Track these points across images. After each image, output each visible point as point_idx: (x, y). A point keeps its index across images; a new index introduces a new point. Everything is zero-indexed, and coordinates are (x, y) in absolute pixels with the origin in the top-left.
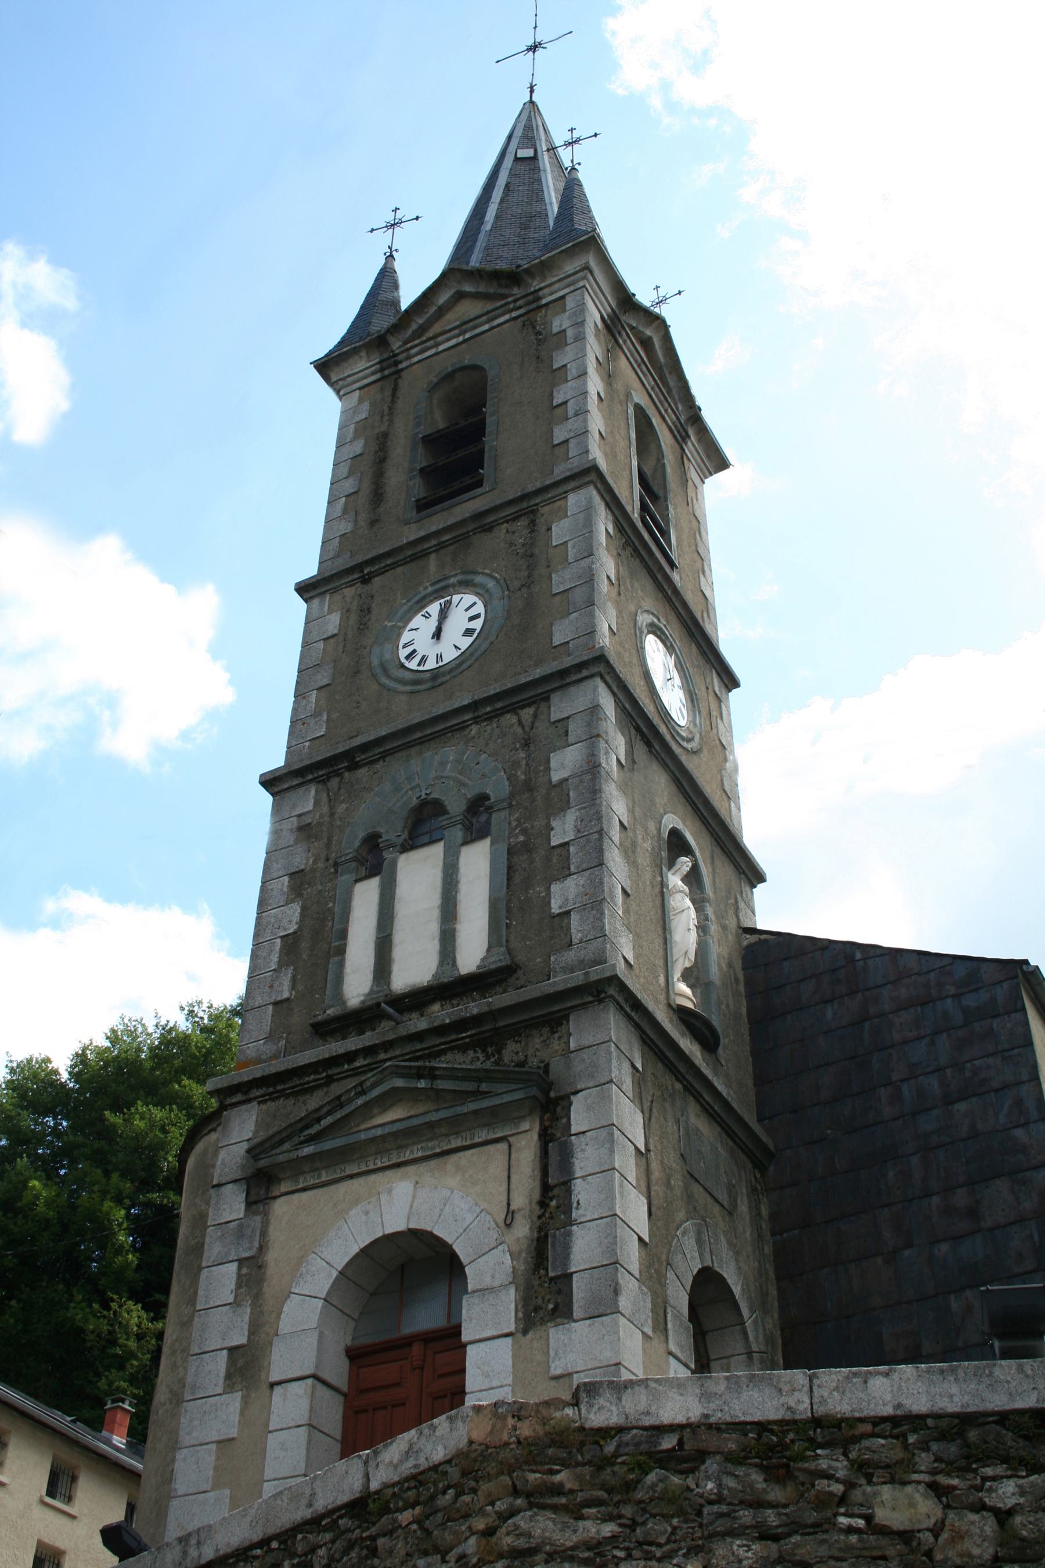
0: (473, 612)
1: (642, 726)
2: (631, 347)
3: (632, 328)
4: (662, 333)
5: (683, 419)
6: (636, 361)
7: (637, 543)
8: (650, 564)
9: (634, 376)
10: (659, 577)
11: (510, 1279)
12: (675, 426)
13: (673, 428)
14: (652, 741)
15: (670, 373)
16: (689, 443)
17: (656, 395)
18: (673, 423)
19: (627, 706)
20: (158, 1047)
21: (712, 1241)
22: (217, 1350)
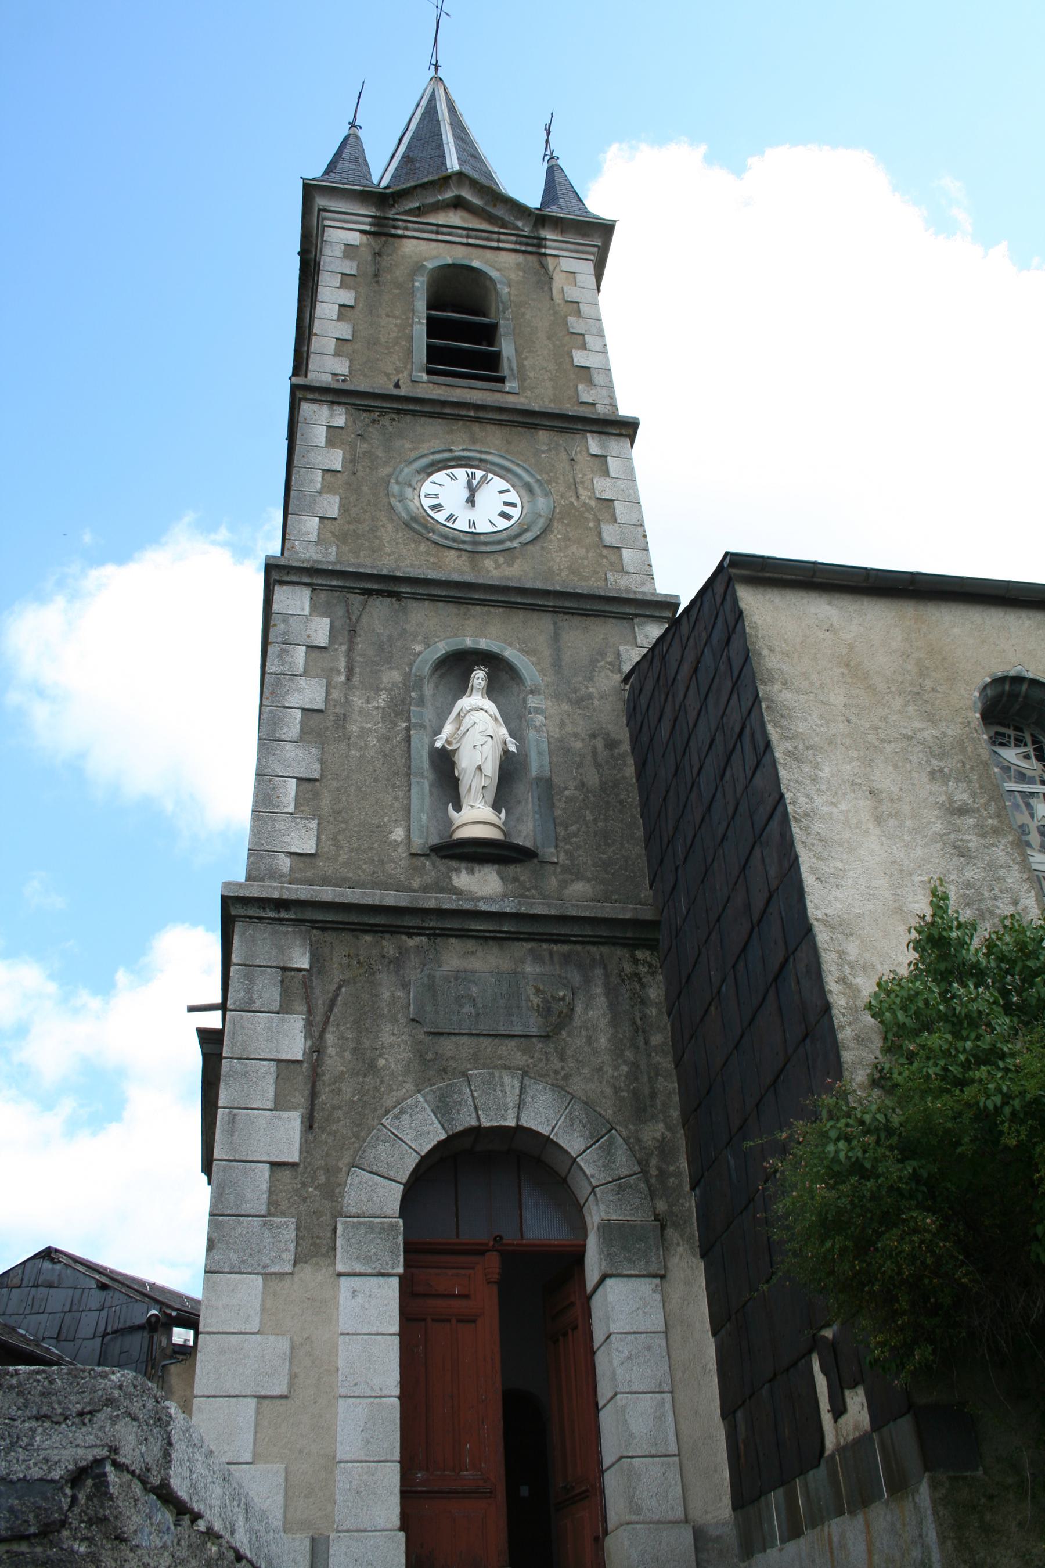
0: (509, 510)
1: (369, 586)
2: (416, 226)
3: (406, 213)
4: (467, 182)
5: (527, 231)
6: (431, 232)
7: (395, 406)
8: (427, 409)
9: (434, 244)
10: (448, 411)
11: (568, 1179)
12: (520, 244)
13: (518, 247)
14: (395, 589)
15: (495, 206)
16: (548, 243)
17: (477, 238)
18: (516, 243)
19: (335, 583)
20: (561, 1029)
21: (476, 1094)
22: (350, 1397)
